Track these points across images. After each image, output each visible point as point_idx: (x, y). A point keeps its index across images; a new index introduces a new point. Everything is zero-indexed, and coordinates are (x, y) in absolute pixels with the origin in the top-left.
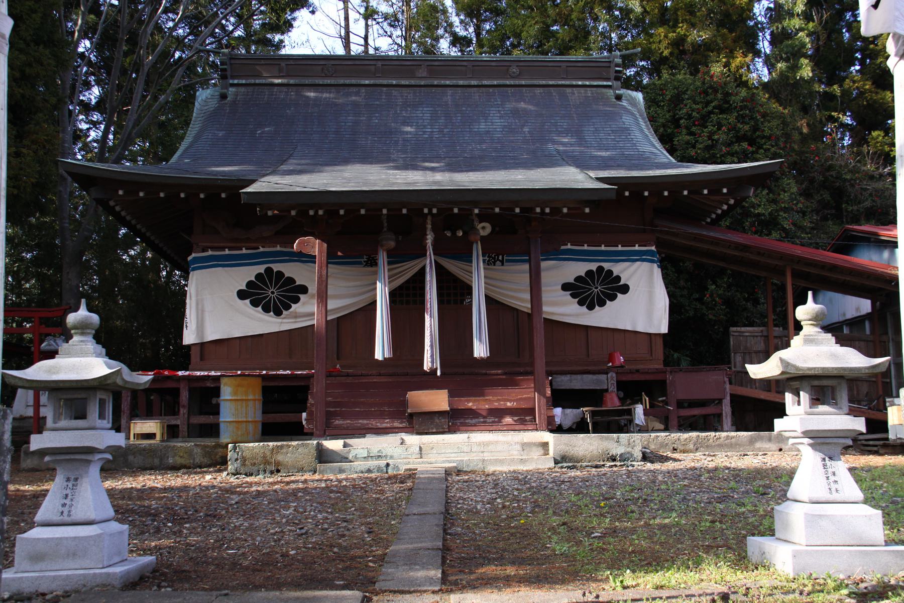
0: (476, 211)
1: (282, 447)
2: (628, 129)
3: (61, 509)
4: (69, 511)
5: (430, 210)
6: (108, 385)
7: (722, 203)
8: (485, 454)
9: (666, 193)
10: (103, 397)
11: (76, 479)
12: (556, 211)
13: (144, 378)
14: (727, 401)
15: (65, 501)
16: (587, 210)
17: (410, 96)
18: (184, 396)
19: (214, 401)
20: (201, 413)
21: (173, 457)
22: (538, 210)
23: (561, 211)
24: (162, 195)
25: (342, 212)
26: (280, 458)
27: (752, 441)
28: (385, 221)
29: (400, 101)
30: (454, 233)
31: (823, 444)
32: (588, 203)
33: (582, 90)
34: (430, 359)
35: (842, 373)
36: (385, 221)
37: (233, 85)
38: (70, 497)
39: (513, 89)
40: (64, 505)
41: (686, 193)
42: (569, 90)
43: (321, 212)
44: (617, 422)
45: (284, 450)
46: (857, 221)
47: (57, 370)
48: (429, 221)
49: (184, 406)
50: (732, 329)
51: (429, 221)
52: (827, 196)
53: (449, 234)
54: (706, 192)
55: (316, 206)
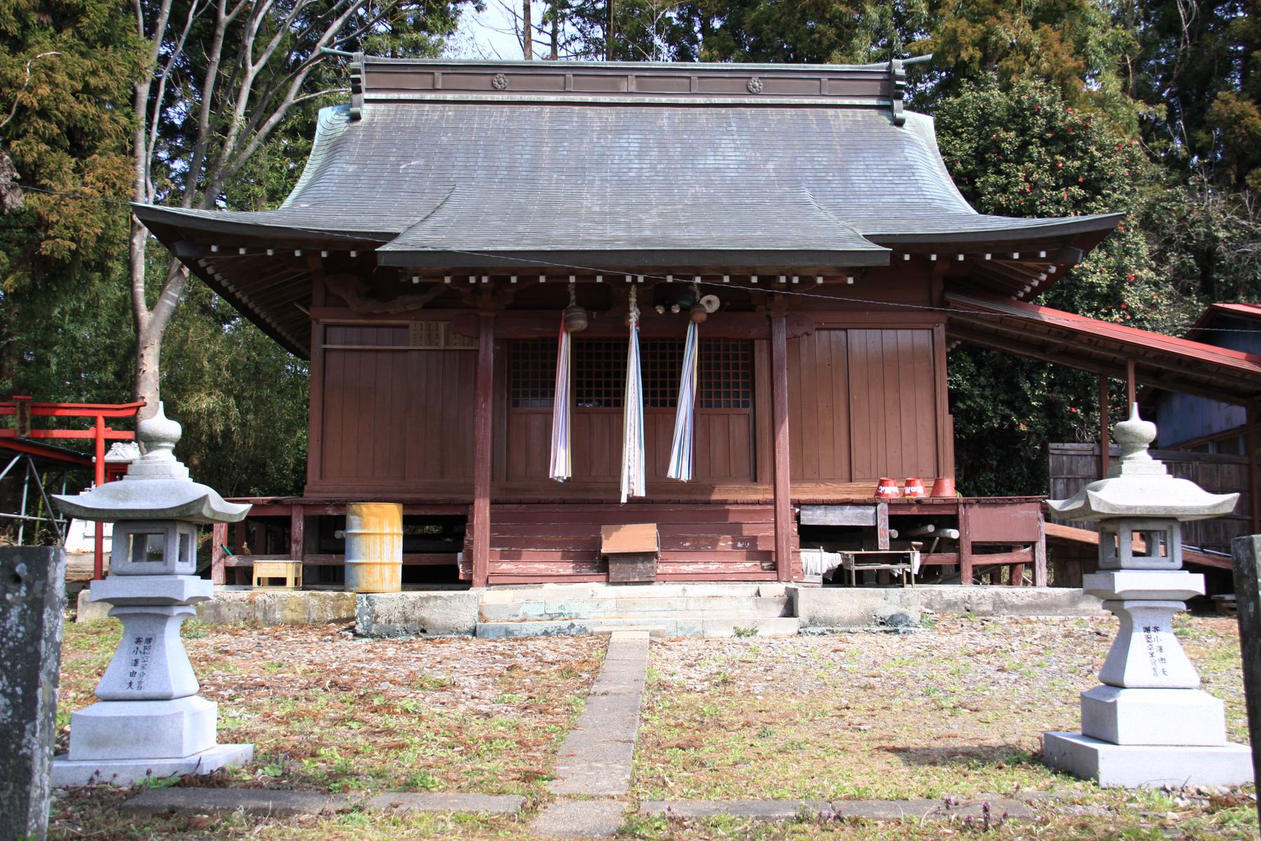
0: (698, 280)
1: (428, 599)
2: (910, 167)
3: (129, 679)
4: (140, 682)
5: (635, 279)
6: (191, 516)
7: (1039, 272)
8: (706, 613)
9: (961, 258)
10: (185, 532)
11: (149, 640)
12: (807, 281)
13: (240, 510)
14: (1041, 546)
15: (135, 669)
16: (850, 281)
17: (612, 118)
18: (298, 527)
19: (338, 534)
20: (321, 551)
21: (282, 610)
22: (783, 279)
23: (815, 281)
24: (270, 252)
25: (514, 280)
26: (425, 614)
27: (1073, 602)
28: (572, 293)
29: (597, 125)
30: (668, 309)
31: (1147, 608)
32: (851, 271)
33: (849, 112)
34: (633, 481)
35: (1174, 513)
36: (572, 293)
37: (367, 101)
38: (140, 663)
39: (753, 110)
40: (133, 674)
41: (988, 257)
42: (831, 111)
43: (485, 280)
44: (889, 573)
45: (431, 604)
46: (1233, 298)
47: (126, 495)
48: (633, 292)
49: (297, 542)
50: (1052, 445)
51: (633, 292)
52: (1190, 260)
53: (660, 311)
54: (1016, 256)
55: (479, 272)
